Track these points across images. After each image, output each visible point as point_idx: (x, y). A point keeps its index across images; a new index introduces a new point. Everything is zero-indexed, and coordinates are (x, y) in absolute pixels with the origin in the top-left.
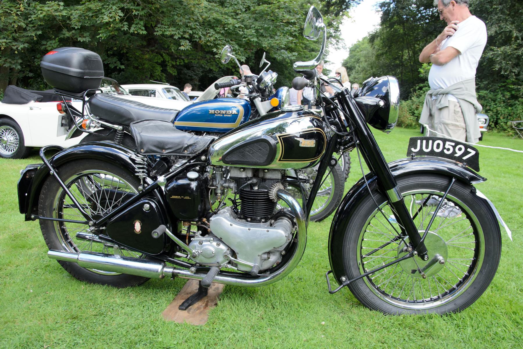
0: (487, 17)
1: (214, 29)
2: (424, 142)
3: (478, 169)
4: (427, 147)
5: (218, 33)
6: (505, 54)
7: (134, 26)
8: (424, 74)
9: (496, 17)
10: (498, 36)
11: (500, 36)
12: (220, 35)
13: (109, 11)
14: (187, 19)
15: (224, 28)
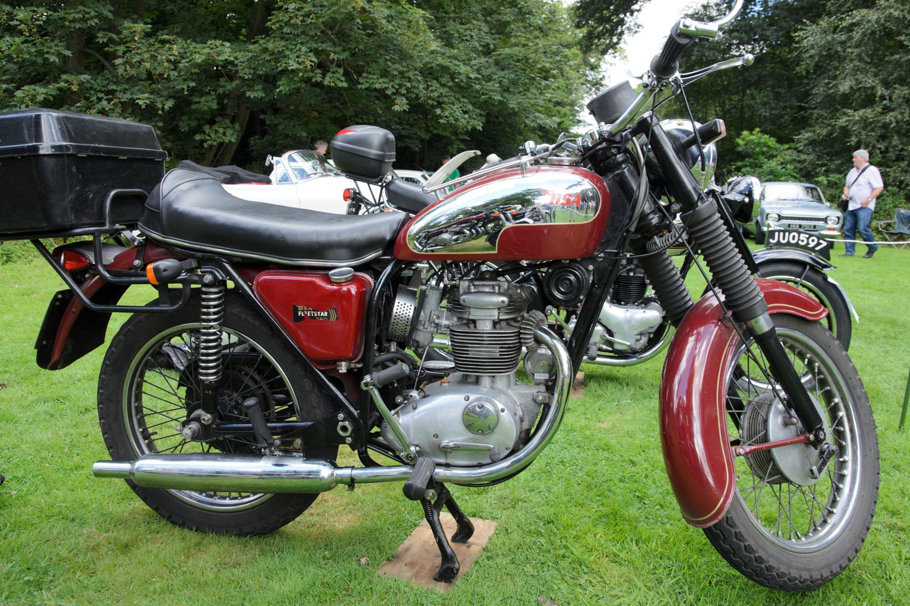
0: (838, 67)
1: (438, 80)
2: (782, 234)
3: (829, 259)
4: (784, 239)
6: (864, 121)
7: (329, 75)
8: (744, 147)
9: (852, 65)
10: (855, 94)
11: (858, 94)
12: (446, 89)
13: (297, 54)
14: (405, 67)
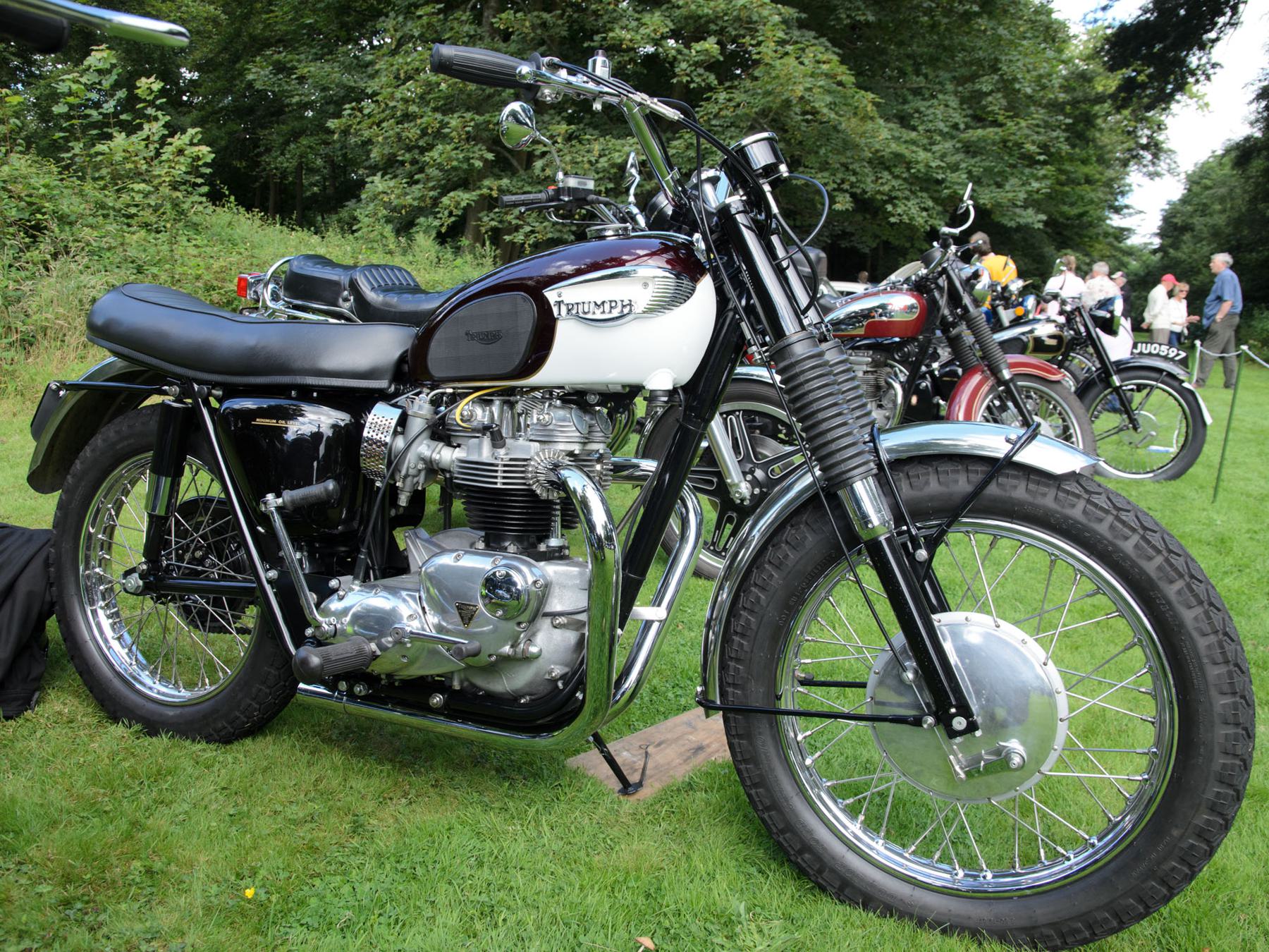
5: (896, 177)
12: (900, 182)
15: (908, 169)
